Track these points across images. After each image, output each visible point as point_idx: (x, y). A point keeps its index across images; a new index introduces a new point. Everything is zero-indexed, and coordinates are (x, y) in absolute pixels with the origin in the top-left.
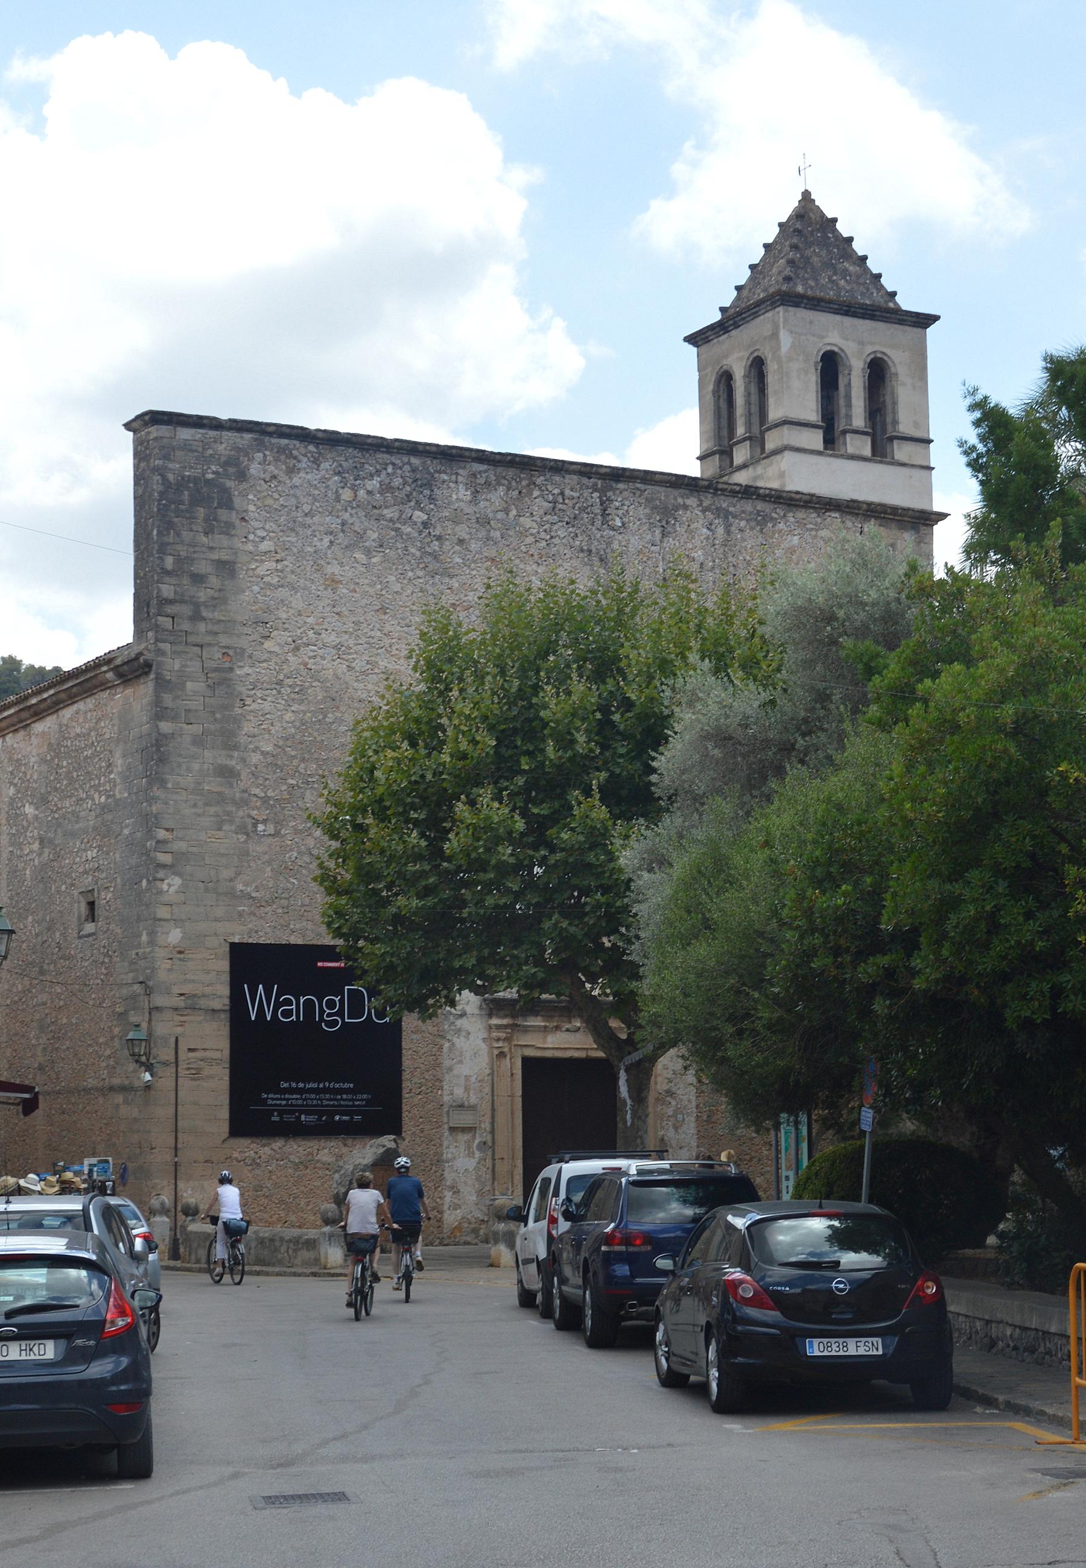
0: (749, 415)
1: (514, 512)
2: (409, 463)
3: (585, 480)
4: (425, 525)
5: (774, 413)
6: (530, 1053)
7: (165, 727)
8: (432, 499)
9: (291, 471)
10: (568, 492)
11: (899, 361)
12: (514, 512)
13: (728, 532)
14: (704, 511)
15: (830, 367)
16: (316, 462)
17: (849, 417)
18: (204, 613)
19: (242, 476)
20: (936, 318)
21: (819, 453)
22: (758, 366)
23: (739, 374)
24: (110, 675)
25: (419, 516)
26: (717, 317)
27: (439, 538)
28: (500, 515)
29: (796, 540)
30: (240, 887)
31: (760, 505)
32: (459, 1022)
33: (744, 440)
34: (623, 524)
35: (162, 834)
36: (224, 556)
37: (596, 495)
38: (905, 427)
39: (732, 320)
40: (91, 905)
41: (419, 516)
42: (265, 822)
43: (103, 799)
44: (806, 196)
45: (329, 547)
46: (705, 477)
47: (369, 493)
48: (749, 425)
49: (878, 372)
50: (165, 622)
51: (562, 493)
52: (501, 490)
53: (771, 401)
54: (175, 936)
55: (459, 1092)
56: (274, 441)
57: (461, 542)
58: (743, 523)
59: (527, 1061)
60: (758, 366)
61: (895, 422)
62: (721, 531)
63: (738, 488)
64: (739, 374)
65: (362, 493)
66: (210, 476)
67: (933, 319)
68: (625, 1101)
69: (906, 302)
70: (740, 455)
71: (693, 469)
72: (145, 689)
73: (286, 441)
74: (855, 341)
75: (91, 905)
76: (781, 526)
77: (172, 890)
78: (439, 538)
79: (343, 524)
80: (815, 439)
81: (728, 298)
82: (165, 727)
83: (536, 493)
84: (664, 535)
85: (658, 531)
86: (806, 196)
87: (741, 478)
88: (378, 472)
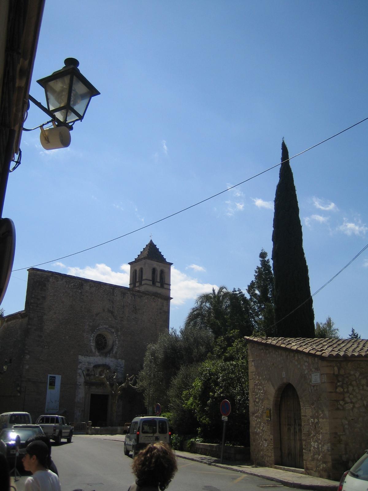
0: (139, 277)
1: (97, 292)
2: (79, 281)
3: (110, 287)
4: (81, 293)
5: (144, 278)
6: (92, 393)
7: (29, 327)
8: (83, 288)
9: (57, 281)
10: (107, 289)
11: (166, 270)
12: (97, 292)
13: (135, 298)
14: (131, 294)
15: (154, 270)
16: (62, 280)
17: (157, 279)
18: (39, 306)
19: (48, 281)
20: (172, 264)
21: (151, 285)
22: (141, 270)
23: (138, 270)
24: (19, 316)
25: (80, 291)
26: (134, 260)
27: (83, 295)
28: (95, 292)
29: (146, 301)
30: (41, 358)
31: (141, 294)
32: (80, 386)
33: (138, 282)
34: (116, 295)
35: (27, 347)
36: (44, 295)
37: (112, 290)
38: (166, 282)
39: (137, 261)
40: (11, 360)
41: (80, 291)
42: (46, 346)
43: (15, 339)
44: (151, 241)
45: (63, 295)
46: (131, 288)
47: (71, 286)
48: (139, 279)
49: (162, 272)
50: (31, 307)
51: (106, 289)
52: (95, 288)
53: (143, 275)
54: (27, 367)
55: (79, 400)
56: (55, 275)
57: (87, 296)
58: (137, 297)
59: (92, 395)
60: (141, 270)
61: (165, 281)
62: (133, 298)
63: (137, 291)
64: (138, 270)
65: (70, 286)
66: (43, 281)
67: (98, 93)
68: (328, 207)
69: (167, 260)
70: (137, 284)
71: (128, 286)
72: (27, 319)
73: (57, 275)
74: (155, 264)
75: (11, 360)
76: (144, 298)
77: (28, 358)
78: (83, 295)
79: (66, 291)
80: (151, 283)
81: (136, 257)
82: (29, 327)
83: (101, 289)
84: (124, 298)
85: (122, 297)
86: (151, 241)
87: (137, 289)
88: (73, 282)
